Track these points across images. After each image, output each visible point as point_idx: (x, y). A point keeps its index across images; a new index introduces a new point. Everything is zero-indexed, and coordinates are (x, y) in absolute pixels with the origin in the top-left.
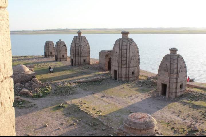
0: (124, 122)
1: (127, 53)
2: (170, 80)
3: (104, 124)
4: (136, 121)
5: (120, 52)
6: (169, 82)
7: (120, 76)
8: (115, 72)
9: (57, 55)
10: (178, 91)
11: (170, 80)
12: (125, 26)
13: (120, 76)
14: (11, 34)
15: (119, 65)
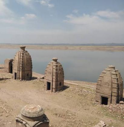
0: (21, 112)
1: (20, 64)
2: (53, 80)
3: (7, 112)
4: (30, 111)
5: (19, 60)
6: (52, 81)
7: (19, 77)
8: (16, 74)
9: (51, 82)
10: (58, 87)
11: (53, 80)
12: (23, 42)
13: (19, 77)
14: (106, 104)
15: (18, 69)
